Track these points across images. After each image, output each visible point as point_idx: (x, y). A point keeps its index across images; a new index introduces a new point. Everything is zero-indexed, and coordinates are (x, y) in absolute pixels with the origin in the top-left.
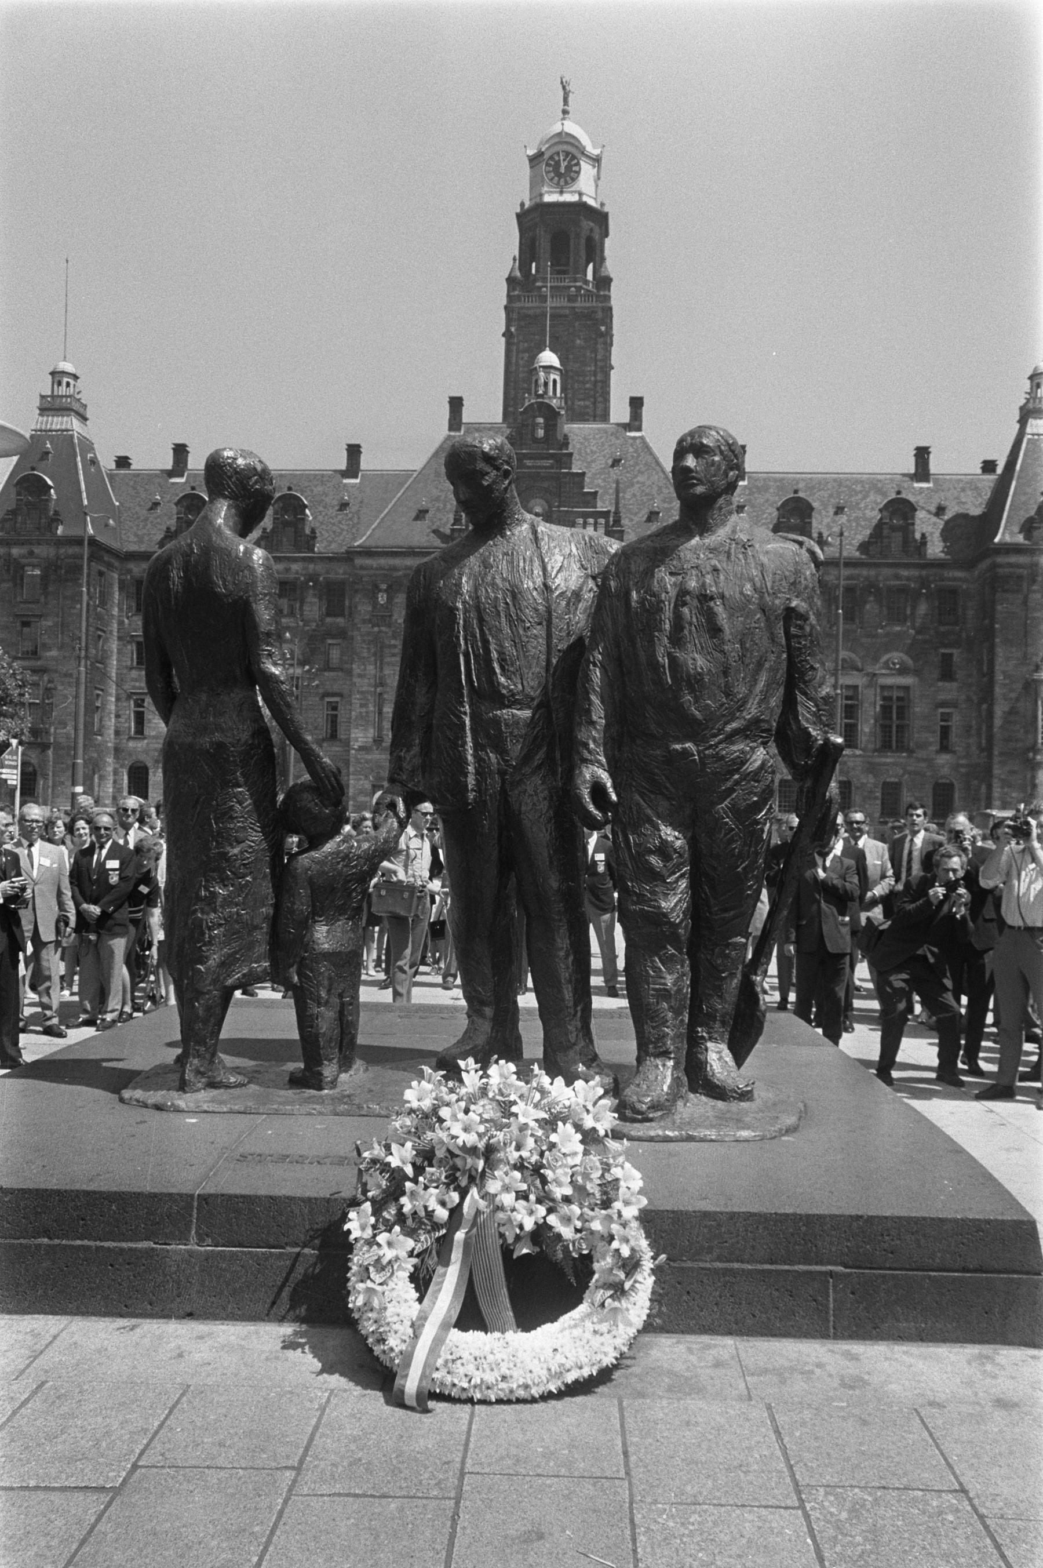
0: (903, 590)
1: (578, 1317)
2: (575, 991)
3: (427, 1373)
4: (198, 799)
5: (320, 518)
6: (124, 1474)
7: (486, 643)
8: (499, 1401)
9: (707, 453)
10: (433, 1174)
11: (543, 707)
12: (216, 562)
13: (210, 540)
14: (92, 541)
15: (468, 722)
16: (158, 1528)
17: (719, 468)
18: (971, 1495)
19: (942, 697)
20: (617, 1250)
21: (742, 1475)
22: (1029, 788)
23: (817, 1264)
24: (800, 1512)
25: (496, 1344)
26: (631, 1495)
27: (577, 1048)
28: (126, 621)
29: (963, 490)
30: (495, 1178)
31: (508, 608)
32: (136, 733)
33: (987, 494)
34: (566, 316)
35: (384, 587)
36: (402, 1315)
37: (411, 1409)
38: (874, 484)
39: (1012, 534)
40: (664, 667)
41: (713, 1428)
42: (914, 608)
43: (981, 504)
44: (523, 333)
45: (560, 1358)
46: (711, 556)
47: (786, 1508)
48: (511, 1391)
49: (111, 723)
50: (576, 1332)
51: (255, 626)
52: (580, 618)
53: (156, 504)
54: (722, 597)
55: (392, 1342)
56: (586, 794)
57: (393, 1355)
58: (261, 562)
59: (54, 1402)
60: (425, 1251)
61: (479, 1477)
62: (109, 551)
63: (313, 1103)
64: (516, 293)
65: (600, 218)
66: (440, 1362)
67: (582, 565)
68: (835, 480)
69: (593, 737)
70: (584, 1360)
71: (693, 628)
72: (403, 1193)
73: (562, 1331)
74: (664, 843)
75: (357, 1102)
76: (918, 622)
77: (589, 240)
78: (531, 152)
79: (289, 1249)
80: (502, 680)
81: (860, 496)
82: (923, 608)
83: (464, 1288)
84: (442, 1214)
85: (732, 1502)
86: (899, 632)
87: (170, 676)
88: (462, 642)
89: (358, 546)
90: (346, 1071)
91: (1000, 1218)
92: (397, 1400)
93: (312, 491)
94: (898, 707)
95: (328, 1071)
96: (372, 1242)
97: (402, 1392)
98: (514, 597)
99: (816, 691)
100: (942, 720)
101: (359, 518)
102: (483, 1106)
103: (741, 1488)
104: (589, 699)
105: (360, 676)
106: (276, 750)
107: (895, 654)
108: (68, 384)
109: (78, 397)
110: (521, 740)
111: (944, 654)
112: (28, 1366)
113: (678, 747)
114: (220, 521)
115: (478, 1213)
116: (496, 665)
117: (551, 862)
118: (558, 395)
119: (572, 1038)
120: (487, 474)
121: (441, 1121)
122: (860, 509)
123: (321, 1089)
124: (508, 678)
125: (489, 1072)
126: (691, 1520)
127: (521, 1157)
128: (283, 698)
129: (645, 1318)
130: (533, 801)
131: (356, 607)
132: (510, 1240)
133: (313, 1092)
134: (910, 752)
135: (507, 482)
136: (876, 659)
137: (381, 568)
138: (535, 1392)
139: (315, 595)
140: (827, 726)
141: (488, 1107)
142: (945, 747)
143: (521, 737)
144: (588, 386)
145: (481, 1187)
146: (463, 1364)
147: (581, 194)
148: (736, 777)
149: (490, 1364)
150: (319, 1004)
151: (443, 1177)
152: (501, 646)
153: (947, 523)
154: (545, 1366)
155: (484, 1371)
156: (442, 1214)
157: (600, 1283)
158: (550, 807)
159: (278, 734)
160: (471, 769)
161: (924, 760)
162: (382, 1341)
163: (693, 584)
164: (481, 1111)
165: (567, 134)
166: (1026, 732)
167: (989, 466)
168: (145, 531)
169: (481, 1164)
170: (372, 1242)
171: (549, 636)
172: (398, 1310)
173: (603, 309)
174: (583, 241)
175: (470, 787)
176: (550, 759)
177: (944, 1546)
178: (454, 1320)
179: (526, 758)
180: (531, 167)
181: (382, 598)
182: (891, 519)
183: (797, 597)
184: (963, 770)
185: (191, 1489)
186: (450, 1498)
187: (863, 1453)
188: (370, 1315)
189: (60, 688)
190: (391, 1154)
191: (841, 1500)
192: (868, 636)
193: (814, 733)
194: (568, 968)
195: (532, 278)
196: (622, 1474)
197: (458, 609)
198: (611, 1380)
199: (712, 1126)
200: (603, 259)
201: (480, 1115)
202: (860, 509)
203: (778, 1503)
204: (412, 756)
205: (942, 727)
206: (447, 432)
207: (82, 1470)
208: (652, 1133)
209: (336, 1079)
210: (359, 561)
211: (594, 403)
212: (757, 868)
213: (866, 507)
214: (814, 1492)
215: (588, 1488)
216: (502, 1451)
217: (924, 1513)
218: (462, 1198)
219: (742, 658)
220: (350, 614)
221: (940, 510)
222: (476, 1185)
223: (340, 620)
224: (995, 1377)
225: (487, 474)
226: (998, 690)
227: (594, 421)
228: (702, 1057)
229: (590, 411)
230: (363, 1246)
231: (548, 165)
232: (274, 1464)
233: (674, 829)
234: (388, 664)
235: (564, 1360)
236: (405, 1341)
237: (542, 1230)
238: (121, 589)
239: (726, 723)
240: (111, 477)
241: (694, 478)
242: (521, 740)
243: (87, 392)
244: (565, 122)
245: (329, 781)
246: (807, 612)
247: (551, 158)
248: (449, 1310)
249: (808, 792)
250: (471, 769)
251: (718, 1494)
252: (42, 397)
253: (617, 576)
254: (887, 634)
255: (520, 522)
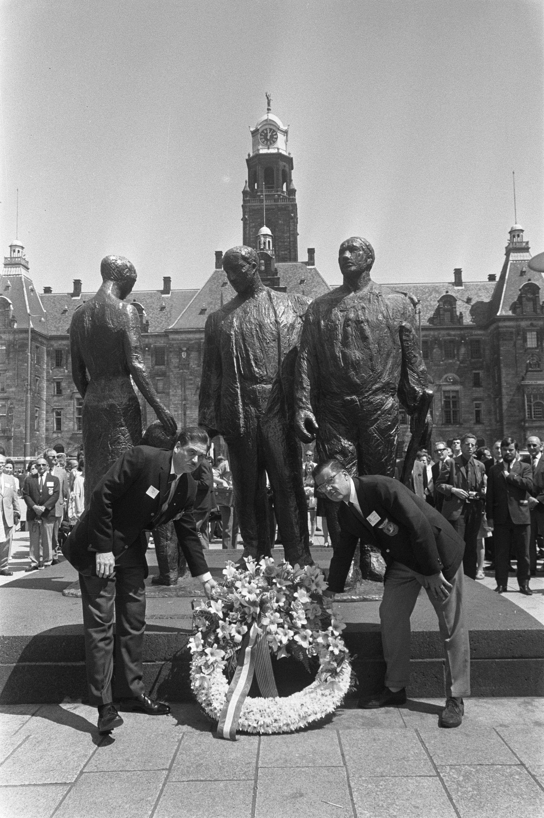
0: (452, 341)
1: (313, 687)
2: (300, 528)
3: (236, 719)
4: (101, 435)
5: (151, 315)
6: (76, 776)
7: (247, 351)
8: (274, 734)
9: (356, 250)
10: (234, 615)
11: (278, 383)
12: (108, 312)
13: (105, 301)
14: (33, 331)
15: (239, 392)
16: (97, 800)
17: (362, 257)
18: (527, 766)
19: (475, 395)
20: (332, 652)
21: (405, 763)
22: (523, 440)
23: (436, 658)
24: (438, 778)
25: (271, 703)
26: (348, 774)
27: (303, 558)
28: (51, 371)
29: (480, 289)
30: (266, 616)
31: (258, 333)
32: (57, 429)
33: (492, 292)
34: (273, 209)
35: (185, 349)
36: (220, 690)
37: (228, 739)
38: (435, 289)
39: (506, 311)
40: (339, 358)
41: (387, 741)
42: (458, 350)
43: (489, 296)
44: (252, 219)
45: (305, 709)
46: (361, 301)
47: (430, 776)
48: (280, 728)
49: (44, 424)
50: (313, 695)
51: (129, 344)
52: (295, 338)
53: (65, 311)
54: (367, 321)
55: (215, 704)
56: (302, 424)
57: (216, 711)
58: (131, 311)
59: (35, 745)
60: (230, 658)
61: (267, 769)
62: (41, 335)
63: (166, 591)
64: (248, 198)
65: (289, 161)
66: (242, 713)
67: (294, 311)
68: (414, 287)
69: (304, 396)
70: (317, 710)
71: (353, 337)
72: (218, 627)
73: (305, 695)
74: (344, 448)
75: (188, 589)
76: (461, 358)
77: (284, 171)
78: (252, 129)
79: (157, 662)
80: (256, 369)
81: (427, 295)
82: (463, 350)
83: (252, 676)
84: (239, 638)
85: (401, 775)
86: (451, 363)
87: (85, 372)
88: (235, 351)
89: (170, 329)
90: (182, 576)
91: (530, 629)
92: (219, 735)
93: (146, 302)
94: (453, 402)
95: (173, 575)
96: (203, 653)
97: (222, 731)
98: (260, 327)
99: (417, 368)
100: (476, 407)
101: (171, 314)
102: (258, 580)
103: (406, 769)
104: (302, 376)
105: (173, 395)
106: (141, 408)
107: (450, 374)
108: (19, 252)
109: (24, 258)
110: (267, 400)
111: (475, 373)
112: (20, 729)
113: (348, 398)
114: (109, 292)
115: (258, 636)
116: (253, 362)
117: (285, 462)
118: (271, 249)
119: (300, 553)
120: (244, 266)
121: (237, 588)
122: (428, 301)
123: (169, 585)
124: (259, 368)
125: (260, 563)
126: (381, 784)
127: (279, 606)
128: (144, 380)
129: (348, 687)
130: (274, 432)
131: (171, 360)
132: (275, 650)
133: (165, 587)
134: (461, 424)
135: (254, 270)
136: (440, 377)
137: (183, 340)
138: (293, 728)
139: (149, 355)
140: (424, 385)
141: (260, 580)
142: (478, 421)
143: (267, 398)
144: (286, 244)
145: (259, 622)
146: (253, 714)
147: (278, 149)
148: (379, 412)
149: (268, 714)
150: (167, 540)
151: (239, 617)
152: (255, 352)
153: (473, 306)
154: (297, 714)
155: (265, 717)
156: (239, 638)
157: (324, 669)
158: (283, 434)
159: (142, 399)
160: (241, 416)
161: (468, 428)
162: (210, 704)
163: (352, 315)
164: (257, 582)
165: (270, 120)
166: (520, 412)
167: (492, 278)
168: (60, 325)
169: (258, 610)
170: (203, 653)
171: (279, 346)
172: (218, 688)
173: (292, 205)
174: (281, 172)
175: (241, 425)
176: (282, 409)
177: (515, 790)
178: (247, 690)
179: (270, 409)
180: (253, 137)
181: (184, 355)
182: (444, 306)
183: (405, 320)
184: (488, 433)
185: (112, 781)
186: (252, 780)
187: (468, 749)
188: (203, 691)
189: (16, 407)
190: (211, 606)
191: (459, 772)
192: (435, 366)
193: (417, 389)
194: (296, 516)
195: (255, 191)
196: (342, 764)
197: (232, 335)
198: (332, 722)
199: (376, 594)
200: (291, 180)
201: (257, 584)
202: (428, 301)
203: (425, 774)
204: (210, 412)
205: (476, 411)
206: (215, 269)
207: (53, 775)
208: (345, 598)
209: (177, 579)
210: (171, 336)
211: (290, 252)
212: (392, 460)
213: (431, 300)
214: (444, 768)
215: (325, 772)
216: (277, 757)
217: (503, 776)
218: (249, 629)
219: (379, 351)
220: (168, 364)
221: (469, 300)
222: (256, 622)
223: (163, 367)
224: (534, 711)
225: (244, 266)
226: (504, 391)
227: (290, 261)
228: (368, 560)
229: (288, 256)
230: (197, 656)
231: (261, 135)
232: (156, 768)
233: (349, 441)
234: (188, 389)
235: (307, 710)
236: (222, 704)
237: (292, 642)
238: (48, 355)
239: (373, 385)
240: (42, 298)
241: (350, 263)
242: (267, 400)
243: (28, 255)
244: (269, 114)
245: (170, 422)
246: (411, 328)
247: (263, 132)
248: (244, 688)
249: (416, 419)
250: (241, 416)
251: (393, 772)
252: (6, 258)
253: (313, 314)
254: (446, 364)
255: (262, 290)
